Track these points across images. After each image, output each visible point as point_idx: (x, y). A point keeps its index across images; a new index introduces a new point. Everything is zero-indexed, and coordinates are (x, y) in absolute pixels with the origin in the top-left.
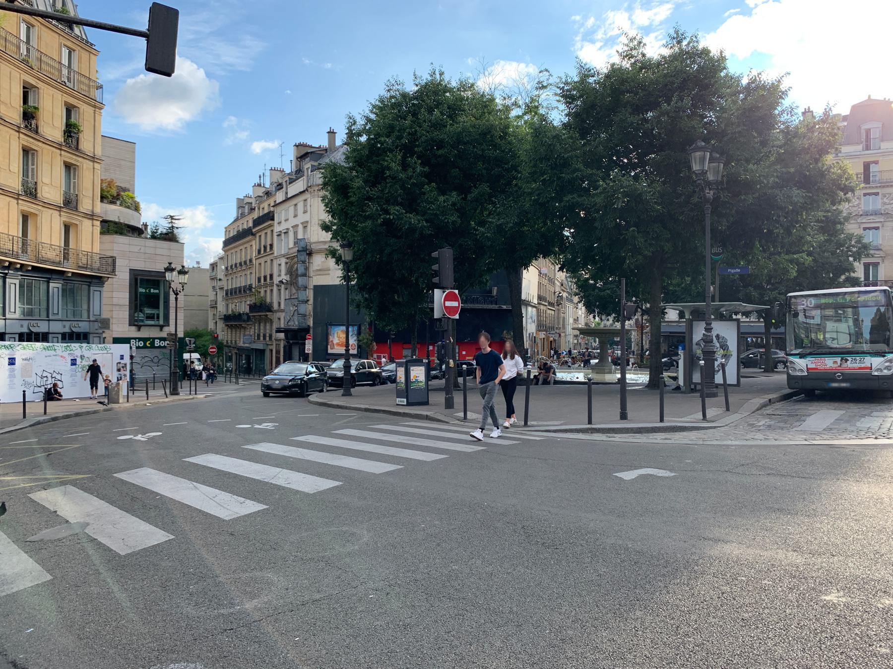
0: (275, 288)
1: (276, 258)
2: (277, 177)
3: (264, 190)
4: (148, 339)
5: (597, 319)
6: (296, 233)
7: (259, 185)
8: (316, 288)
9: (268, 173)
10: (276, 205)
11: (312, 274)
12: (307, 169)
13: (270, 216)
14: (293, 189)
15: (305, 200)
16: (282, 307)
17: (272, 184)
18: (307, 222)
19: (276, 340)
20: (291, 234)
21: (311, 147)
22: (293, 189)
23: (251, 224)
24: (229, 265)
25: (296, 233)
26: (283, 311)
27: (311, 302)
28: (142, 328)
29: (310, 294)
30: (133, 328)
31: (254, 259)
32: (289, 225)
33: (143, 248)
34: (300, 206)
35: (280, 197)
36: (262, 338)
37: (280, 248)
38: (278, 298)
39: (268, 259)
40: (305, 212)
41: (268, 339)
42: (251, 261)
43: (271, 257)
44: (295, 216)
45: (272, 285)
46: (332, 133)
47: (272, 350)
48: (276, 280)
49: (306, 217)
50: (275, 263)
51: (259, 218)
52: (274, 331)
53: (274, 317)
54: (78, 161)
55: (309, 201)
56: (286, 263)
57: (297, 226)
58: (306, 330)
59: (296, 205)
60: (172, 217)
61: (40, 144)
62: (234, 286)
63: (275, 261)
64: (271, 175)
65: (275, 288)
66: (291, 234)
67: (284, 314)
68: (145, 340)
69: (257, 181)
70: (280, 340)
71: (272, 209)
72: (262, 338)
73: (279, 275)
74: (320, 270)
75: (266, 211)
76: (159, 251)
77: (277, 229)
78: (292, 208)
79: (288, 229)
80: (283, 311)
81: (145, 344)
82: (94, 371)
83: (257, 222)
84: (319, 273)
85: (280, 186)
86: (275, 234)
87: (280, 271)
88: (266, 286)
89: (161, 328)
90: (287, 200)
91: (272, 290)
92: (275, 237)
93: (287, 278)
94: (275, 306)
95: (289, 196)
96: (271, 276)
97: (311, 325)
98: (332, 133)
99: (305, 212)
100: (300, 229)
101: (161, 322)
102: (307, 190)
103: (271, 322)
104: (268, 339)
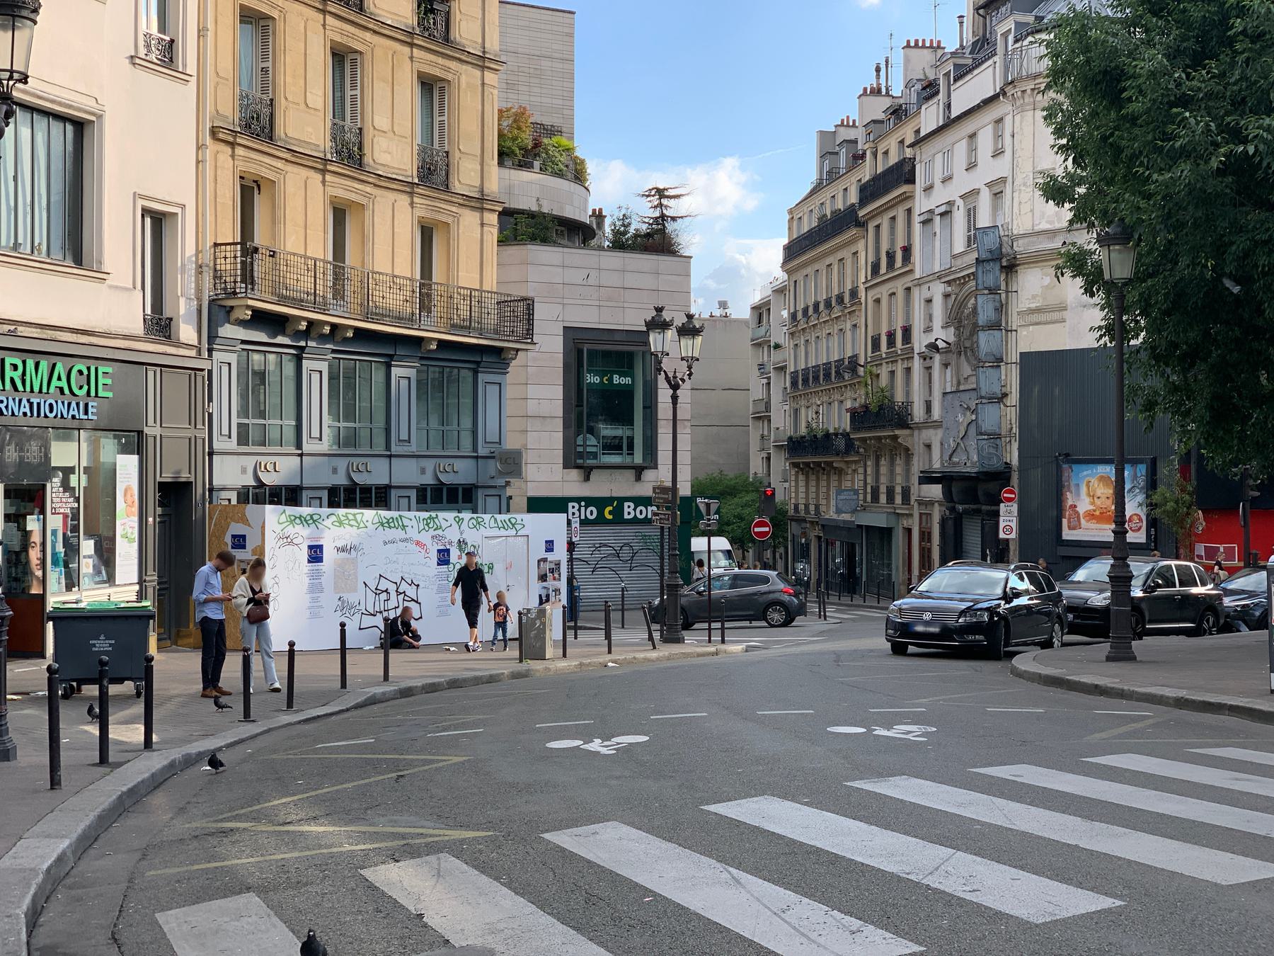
0: (917, 364)
1: (919, 283)
7: (876, 92)
9: (898, 58)
10: (919, 141)
11: (1015, 321)
15: (999, 121)
16: (936, 413)
18: (1003, 180)
19: (920, 503)
20: (959, 217)
22: (966, 94)
23: (853, 198)
25: (971, 214)
26: (937, 425)
27: (1014, 398)
28: (595, 475)
29: (1012, 378)
30: (574, 474)
35: (930, 117)
36: (883, 499)
38: (923, 390)
39: (899, 286)
40: (998, 153)
41: (898, 499)
42: (854, 293)
43: (906, 282)
47: (909, 531)
48: (920, 342)
49: (1000, 168)
50: (918, 296)
51: (876, 179)
52: (915, 480)
54: (448, 69)
56: (947, 296)
57: (975, 193)
58: (1000, 477)
59: (972, 136)
60: (661, 193)
61: (368, 36)
62: (812, 363)
63: (916, 292)
64: (907, 61)
66: (959, 217)
67: (940, 433)
68: (600, 503)
69: (870, 81)
70: (931, 503)
71: (909, 153)
72: (883, 499)
73: (928, 330)
74: (1038, 310)
75: (893, 159)
76: (631, 280)
77: (922, 204)
80: (937, 425)
81: (601, 513)
83: (870, 191)
84: (1035, 318)
85: (929, 90)
86: (917, 219)
87: (930, 318)
89: (639, 471)
90: (949, 124)
92: (917, 228)
94: (918, 413)
95: (954, 114)
96: (907, 331)
97: (1015, 461)
99: (998, 153)
100: (985, 199)
101: (638, 459)
102: (1003, 92)
104: (898, 499)
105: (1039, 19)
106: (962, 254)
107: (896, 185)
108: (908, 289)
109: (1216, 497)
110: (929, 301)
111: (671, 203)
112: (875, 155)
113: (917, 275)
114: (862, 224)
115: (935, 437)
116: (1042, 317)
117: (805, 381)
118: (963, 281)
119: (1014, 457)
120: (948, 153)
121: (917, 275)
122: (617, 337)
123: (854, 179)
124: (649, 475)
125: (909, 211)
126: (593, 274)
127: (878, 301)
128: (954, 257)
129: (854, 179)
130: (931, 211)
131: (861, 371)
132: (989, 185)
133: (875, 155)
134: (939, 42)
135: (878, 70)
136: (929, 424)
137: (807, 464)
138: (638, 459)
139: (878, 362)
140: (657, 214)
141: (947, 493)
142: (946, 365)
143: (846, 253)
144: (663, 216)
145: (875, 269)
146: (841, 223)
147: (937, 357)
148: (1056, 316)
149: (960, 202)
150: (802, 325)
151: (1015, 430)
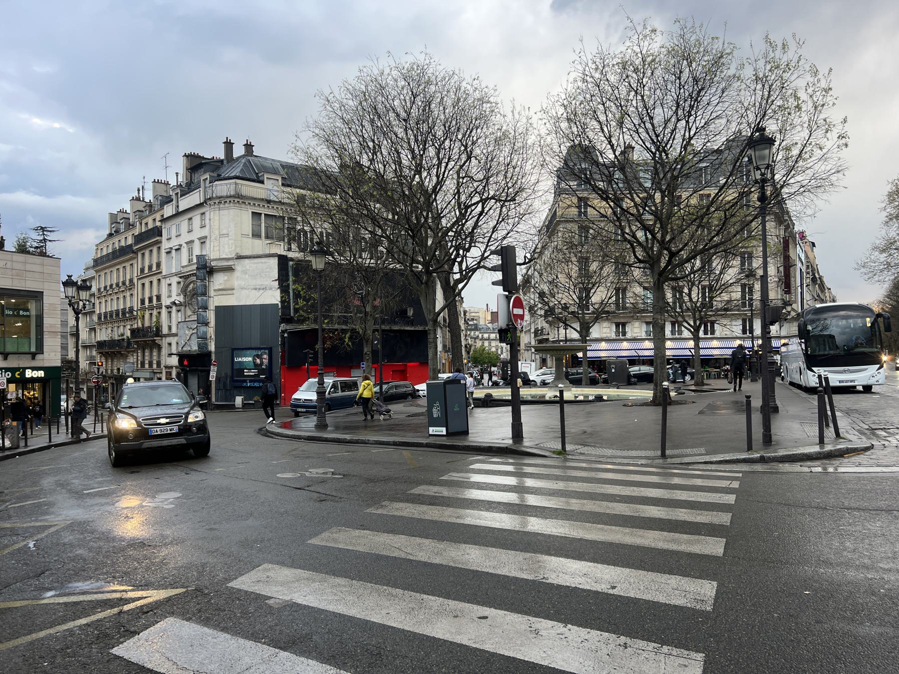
0: (164, 311)
1: (165, 277)
2: (162, 190)
3: (144, 204)
4: (18, 369)
5: (92, 465)
6: (190, 251)
7: (138, 199)
8: (218, 309)
9: (149, 186)
10: (164, 220)
11: (212, 293)
12: (205, 180)
13: (157, 232)
14: (186, 202)
15: (203, 214)
16: (174, 330)
17: (155, 197)
18: (206, 237)
19: (166, 367)
20: (184, 250)
21: (203, 158)
22: (186, 202)
23: (130, 241)
24: (108, 284)
25: (190, 251)
26: (176, 335)
27: (212, 323)
28: (10, 356)
29: (211, 316)
31: (135, 280)
32: (174, 243)
33: (9, 264)
34: (197, 221)
35: (169, 210)
36: (147, 366)
37: (169, 267)
38: (171, 321)
39: (155, 279)
40: (203, 227)
41: (155, 366)
42: (131, 281)
43: (159, 277)
44: (190, 231)
45: (160, 307)
46: (229, 145)
48: (166, 301)
49: (205, 232)
50: (164, 283)
51: (141, 234)
53: (164, 342)
55: (207, 214)
56: (179, 283)
57: (192, 242)
59: (190, 219)
60: (43, 229)
62: (109, 309)
63: (163, 281)
64: (154, 188)
65: (164, 311)
66: (184, 250)
67: (176, 338)
68: (13, 370)
69: (135, 194)
70: (171, 367)
71: (158, 224)
72: (147, 366)
73: (170, 296)
74: (220, 290)
75: (150, 226)
76: (29, 267)
77: (165, 245)
78: (198, 217)
79: (181, 245)
80: (176, 335)
81: (13, 375)
82: (821, 149)
83: (139, 238)
84: (221, 292)
85: (167, 200)
86: (163, 252)
87: (170, 291)
88: (151, 308)
89: (33, 356)
90: (178, 214)
91: (159, 313)
92: (163, 254)
93: (181, 299)
94: (165, 331)
95: (181, 209)
96: (159, 298)
98: (229, 145)
99: (203, 227)
100: (197, 244)
101: (33, 349)
102: (205, 202)
103: (159, 348)
104: (155, 366)
105: (219, 175)
106: (186, 266)
107: (153, 236)
108: (159, 280)
109: (424, 362)
110: (170, 285)
111: (49, 233)
112: (141, 224)
113: (164, 274)
114: (135, 252)
115: (174, 340)
116: (224, 292)
117: (105, 317)
118: (186, 277)
119: (212, 347)
120: (178, 227)
121: (164, 274)
122: (22, 293)
123: (130, 234)
124: (39, 357)
125: (159, 248)
126: (9, 264)
127: (143, 284)
128: (183, 267)
129: (130, 234)
130: (171, 248)
131: (135, 313)
132: (199, 239)
133: (141, 224)
134: (249, 147)
135: (139, 190)
136: (170, 335)
137: (107, 353)
138: (33, 349)
139: (143, 309)
140: (42, 238)
141: (180, 361)
142: (178, 311)
143: (127, 265)
144: (45, 239)
145: (142, 270)
146: (123, 253)
147: (174, 308)
148: (230, 292)
149: (185, 245)
150: (104, 294)
151: (213, 337)
